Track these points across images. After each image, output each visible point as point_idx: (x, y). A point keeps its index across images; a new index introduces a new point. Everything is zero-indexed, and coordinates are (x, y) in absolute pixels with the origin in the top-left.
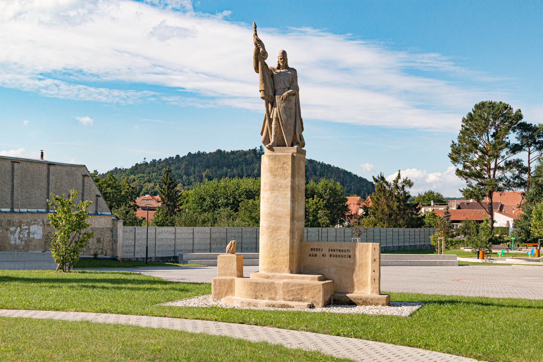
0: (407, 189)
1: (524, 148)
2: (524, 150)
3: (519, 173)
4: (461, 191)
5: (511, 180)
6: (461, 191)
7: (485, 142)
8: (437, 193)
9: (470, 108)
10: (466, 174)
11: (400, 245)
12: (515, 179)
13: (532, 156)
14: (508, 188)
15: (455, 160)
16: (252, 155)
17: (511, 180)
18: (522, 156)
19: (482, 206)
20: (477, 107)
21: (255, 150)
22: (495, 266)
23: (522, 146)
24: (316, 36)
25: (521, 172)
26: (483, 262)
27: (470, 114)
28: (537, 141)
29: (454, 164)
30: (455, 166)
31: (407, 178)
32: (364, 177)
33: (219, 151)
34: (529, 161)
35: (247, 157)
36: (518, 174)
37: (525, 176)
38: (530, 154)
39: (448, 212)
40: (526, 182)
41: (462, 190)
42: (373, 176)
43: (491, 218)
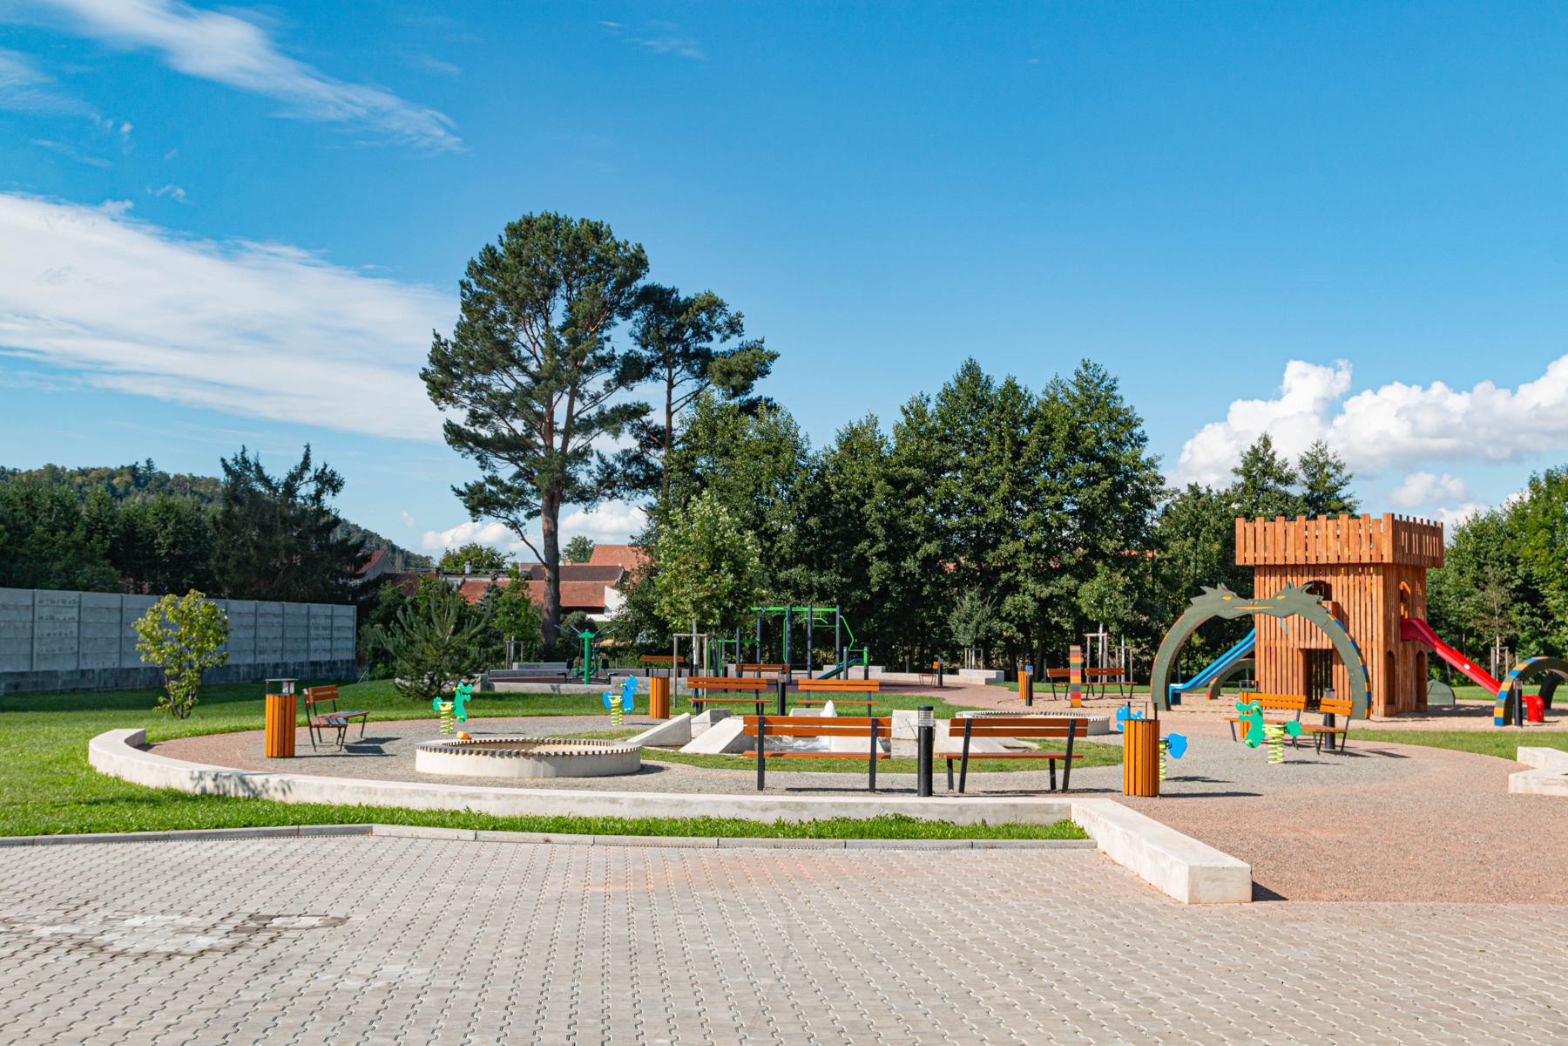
0: (328, 500)
1: (655, 370)
2: (657, 377)
3: (641, 445)
4: (460, 493)
5: (618, 466)
6: (460, 493)
7: (537, 342)
8: (488, 549)
9: (492, 234)
10: (479, 440)
11: (83, 667)
12: (629, 463)
13: (677, 393)
14: (609, 492)
15: (440, 391)
16: (128, 478)
17: (618, 466)
18: (648, 392)
19: (523, 539)
20: (512, 230)
21: (134, 469)
22: (265, 845)
23: (650, 365)
24: (308, 265)
25: (645, 445)
26: (198, 791)
27: (490, 250)
28: (692, 350)
29: (437, 403)
30: (440, 409)
31: (326, 466)
32: (373, 530)
33: (52, 469)
34: (669, 406)
35: (115, 482)
36: (638, 449)
37: (657, 458)
38: (671, 386)
39: (494, 586)
40: (659, 474)
41: (463, 489)
42: (223, 460)
43: (552, 578)
